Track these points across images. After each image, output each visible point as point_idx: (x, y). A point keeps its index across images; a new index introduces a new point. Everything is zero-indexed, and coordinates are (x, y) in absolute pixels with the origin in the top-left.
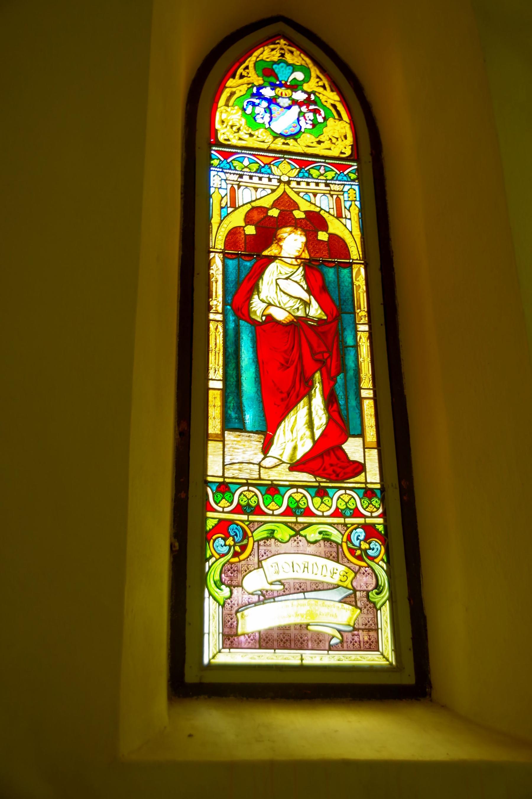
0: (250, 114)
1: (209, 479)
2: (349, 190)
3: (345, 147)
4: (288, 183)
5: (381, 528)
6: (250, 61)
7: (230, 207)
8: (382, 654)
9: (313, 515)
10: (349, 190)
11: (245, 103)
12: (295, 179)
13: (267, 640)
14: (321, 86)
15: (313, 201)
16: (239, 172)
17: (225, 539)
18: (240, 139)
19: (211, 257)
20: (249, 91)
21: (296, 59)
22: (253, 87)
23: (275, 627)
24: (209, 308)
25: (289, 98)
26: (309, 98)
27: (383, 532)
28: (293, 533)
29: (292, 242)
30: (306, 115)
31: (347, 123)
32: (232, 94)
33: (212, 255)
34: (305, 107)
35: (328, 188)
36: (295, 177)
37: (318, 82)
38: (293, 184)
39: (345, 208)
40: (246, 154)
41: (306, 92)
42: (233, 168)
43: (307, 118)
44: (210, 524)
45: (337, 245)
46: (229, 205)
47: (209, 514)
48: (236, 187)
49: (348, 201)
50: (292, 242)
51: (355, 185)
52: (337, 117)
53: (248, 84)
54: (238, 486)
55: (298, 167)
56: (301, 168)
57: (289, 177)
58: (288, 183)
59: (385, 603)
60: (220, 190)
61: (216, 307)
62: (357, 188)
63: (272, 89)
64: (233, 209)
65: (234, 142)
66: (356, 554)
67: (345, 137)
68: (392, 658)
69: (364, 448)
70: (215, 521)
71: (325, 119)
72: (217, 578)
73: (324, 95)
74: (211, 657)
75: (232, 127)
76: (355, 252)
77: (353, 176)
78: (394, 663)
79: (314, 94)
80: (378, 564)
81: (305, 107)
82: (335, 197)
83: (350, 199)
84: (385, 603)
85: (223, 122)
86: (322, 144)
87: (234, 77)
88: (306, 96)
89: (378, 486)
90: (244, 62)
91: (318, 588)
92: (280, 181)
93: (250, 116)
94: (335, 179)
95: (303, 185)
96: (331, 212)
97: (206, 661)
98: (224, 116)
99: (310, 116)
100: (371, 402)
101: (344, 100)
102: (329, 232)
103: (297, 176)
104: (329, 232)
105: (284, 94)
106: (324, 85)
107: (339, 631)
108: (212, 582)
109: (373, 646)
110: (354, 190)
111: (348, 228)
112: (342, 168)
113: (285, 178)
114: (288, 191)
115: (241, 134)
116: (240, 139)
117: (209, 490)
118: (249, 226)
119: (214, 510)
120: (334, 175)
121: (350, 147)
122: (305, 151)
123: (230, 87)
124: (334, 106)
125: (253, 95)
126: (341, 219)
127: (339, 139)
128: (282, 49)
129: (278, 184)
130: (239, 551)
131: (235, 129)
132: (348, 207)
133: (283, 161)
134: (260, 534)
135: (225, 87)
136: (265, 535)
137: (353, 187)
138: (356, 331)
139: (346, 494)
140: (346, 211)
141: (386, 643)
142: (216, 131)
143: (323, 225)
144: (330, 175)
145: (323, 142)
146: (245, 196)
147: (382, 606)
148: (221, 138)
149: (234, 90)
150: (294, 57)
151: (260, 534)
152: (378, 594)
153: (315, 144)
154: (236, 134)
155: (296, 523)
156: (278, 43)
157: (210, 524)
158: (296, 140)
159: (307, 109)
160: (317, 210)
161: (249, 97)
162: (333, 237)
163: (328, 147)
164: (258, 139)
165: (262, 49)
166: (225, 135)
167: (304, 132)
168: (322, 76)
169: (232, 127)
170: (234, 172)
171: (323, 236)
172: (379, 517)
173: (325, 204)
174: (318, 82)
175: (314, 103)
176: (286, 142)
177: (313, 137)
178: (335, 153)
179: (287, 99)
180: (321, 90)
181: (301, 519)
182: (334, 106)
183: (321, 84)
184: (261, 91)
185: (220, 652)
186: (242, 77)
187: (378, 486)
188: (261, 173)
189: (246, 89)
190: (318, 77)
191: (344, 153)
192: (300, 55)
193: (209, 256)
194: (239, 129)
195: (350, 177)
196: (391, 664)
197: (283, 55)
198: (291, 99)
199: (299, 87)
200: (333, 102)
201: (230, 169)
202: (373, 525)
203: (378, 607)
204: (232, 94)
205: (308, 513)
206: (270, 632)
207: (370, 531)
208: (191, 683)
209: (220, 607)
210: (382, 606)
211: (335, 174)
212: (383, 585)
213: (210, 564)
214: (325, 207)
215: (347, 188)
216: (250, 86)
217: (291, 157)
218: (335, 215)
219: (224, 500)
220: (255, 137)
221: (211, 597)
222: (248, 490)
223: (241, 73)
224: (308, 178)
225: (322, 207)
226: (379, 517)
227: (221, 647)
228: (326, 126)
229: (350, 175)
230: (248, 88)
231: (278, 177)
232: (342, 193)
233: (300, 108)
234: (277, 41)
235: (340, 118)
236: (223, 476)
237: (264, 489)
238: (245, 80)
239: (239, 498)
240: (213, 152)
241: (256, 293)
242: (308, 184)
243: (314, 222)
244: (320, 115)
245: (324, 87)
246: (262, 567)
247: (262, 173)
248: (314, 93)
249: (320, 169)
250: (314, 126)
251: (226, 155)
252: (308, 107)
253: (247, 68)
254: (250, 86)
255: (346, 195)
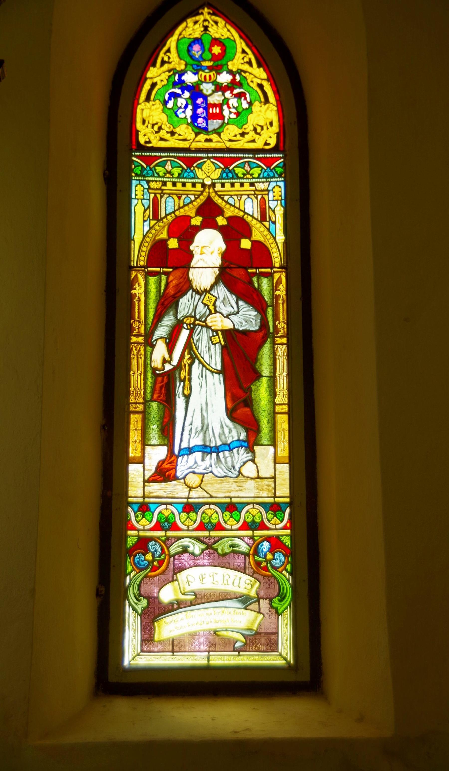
0: (172, 108)
1: (130, 500)
2: (274, 187)
3: (270, 137)
4: (213, 185)
5: (287, 541)
6: (172, 42)
7: (153, 219)
8: (280, 655)
9: (223, 529)
10: (274, 187)
11: (167, 96)
12: (218, 181)
13: (179, 645)
14: (247, 63)
15: (237, 205)
16: (162, 179)
17: (144, 555)
18: (162, 139)
19: (133, 276)
20: (170, 79)
21: (220, 31)
22: (174, 74)
23: (186, 633)
24: (131, 329)
25: (212, 83)
26: (233, 81)
27: (289, 546)
28: (203, 547)
29: (208, 247)
30: (231, 102)
31: (274, 105)
32: (154, 85)
33: (134, 274)
34: (229, 92)
35: (253, 188)
36: (218, 179)
37: (243, 59)
38: (218, 187)
39: (270, 207)
40: (168, 156)
41: (230, 72)
42: (156, 175)
43: (231, 106)
44: (131, 542)
45: (261, 252)
46: (151, 218)
47: (130, 533)
48: (159, 196)
49: (273, 200)
50: (208, 247)
51: (280, 181)
52: (263, 100)
53: (169, 71)
54: (157, 505)
55: (222, 166)
56: (226, 167)
57: (212, 179)
58: (213, 185)
59: (286, 608)
60: (143, 201)
61: (138, 329)
62: (282, 184)
63: (195, 74)
64: (155, 221)
65: (155, 143)
66: (262, 565)
67: (271, 124)
68: (290, 657)
69: (275, 463)
70: (136, 539)
71: (250, 104)
72: (136, 591)
73: (250, 74)
74: (131, 658)
75: (153, 125)
76: (277, 259)
77: (279, 170)
78: (292, 662)
79: (240, 74)
80: (281, 573)
81: (229, 92)
82: (259, 197)
83: (275, 198)
84: (286, 608)
85: (144, 122)
86: (246, 136)
87: (154, 65)
88: (230, 78)
89: (288, 500)
90: (164, 45)
91: (226, 597)
92: (203, 185)
93: (171, 111)
94: (261, 176)
95: (228, 186)
96: (256, 215)
97: (126, 663)
98: (146, 114)
99: (233, 102)
100: (286, 417)
101: (271, 78)
102: (252, 239)
103: (221, 178)
104: (252, 239)
105: (208, 78)
106: (250, 60)
107: (243, 635)
108: (132, 595)
109: (271, 645)
110: (280, 187)
111: (274, 236)
112: (268, 162)
113: (208, 182)
114: (213, 195)
115: (163, 133)
116: (162, 139)
117: (130, 509)
118: (172, 239)
119: (134, 528)
120: (260, 172)
121: (276, 135)
122: (228, 146)
123: (152, 78)
124: (261, 86)
125: (175, 84)
126: (264, 223)
127: (265, 128)
128: (205, 20)
129: (202, 189)
130: (158, 565)
131: (156, 128)
132: (273, 207)
133: (205, 162)
134: (174, 549)
135: (146, 79)
136: (180, 549)
137: (279, 184)
138: (274, 343)
139: (253, 508)
140: (271, 213)
141: (285, 644)
142: (138, 132)
143: (247, 231)
144: (256, 172)
145: (248, 133)
146: (168, 206)
147: (283, 611)
148: (142, 140)
149: (155, 80)
150: (210, 26)
151: (174, 549)
152: (281, 601)
153: (239, 137)
154: (157, 135)
155: (210, 537)
156: (202, 14)
157: (131, 542)
158: (219, 134)
159: (231, 95)
160: (241, 214)
161: (171, 86)
162: (257, 244)
163: (252, 139)
164: (181, 137)
165: (184, 24)
166: (146, 137)
167: (228, 124)
168: (247, 50)
169: (153, 125)
170: (158, 179)
171: (246, 244)
172: (285, 528)
173: (251, 207)
174: (243, 59)
175: (240, 85)
176: (208, 137)
177: (236, 128)
178: (259, 144)
179: (210, 85)
180: (246, 67)
181: (213, 533)
182: (261, 86)
183: (246, 60)
184: (183, 78)
185: (138, 655)
186: (163, 63)
187: (288, 500)
188: (183, 178)
189: (167, 78)
190: (244, 52)
191: (269, 144)
192: (225, 26)
193: (130, 275)
194: (160, 128)
195: (276, 172)
196: (288, 663)
197: (206, 28)
198: (214, 83)
199: (225, 68)
200: (259, 82)
201: (153, 176)
202: (277, 538)
203: (280, 612)
204: (154, 85)
205: (218, 527)
206: (182, 638)
207: (276, 544)
208: (113, 682)
209: (139, 617)
210: (283, 611)
211: (261, 170)
212: (285, 592)
213: (131, 577)
214: (249, 210)
215: (273, 184)
216: (172, 73)
217: (215, 155)
218: (259, 219)
219: (144, 519)
220: (176, 135)
221: (131, 608)
222: (167, 509)
223: (163, 58)
224: (233, 178)
225: (246, 211)
226: (285, 528)
227: (139, 651)
228: (252, 112)
229: (277, 169)
230: (169, 77)
231: (201, 181)
232: (267, 192)
233: (223, 95)
234: (200, 12)
235: (267, 101)
236: (144, 497)
237: (180, 507)
238: (166, 67)
239: (158, 516)
240: (134, 158)
241: (174, 306)
242: (233, 185)
243: (235, 229)
244: (245, 99)
245: (250, 63)
246: (177, 580)
247: (186, 178)
248: (240, 72)
249: (245, 166)
250: (238, 114)
251: (149, 161)
252: (232, 92)
253: (169, 51)
254: (172, 73)
255: (271, 194)
